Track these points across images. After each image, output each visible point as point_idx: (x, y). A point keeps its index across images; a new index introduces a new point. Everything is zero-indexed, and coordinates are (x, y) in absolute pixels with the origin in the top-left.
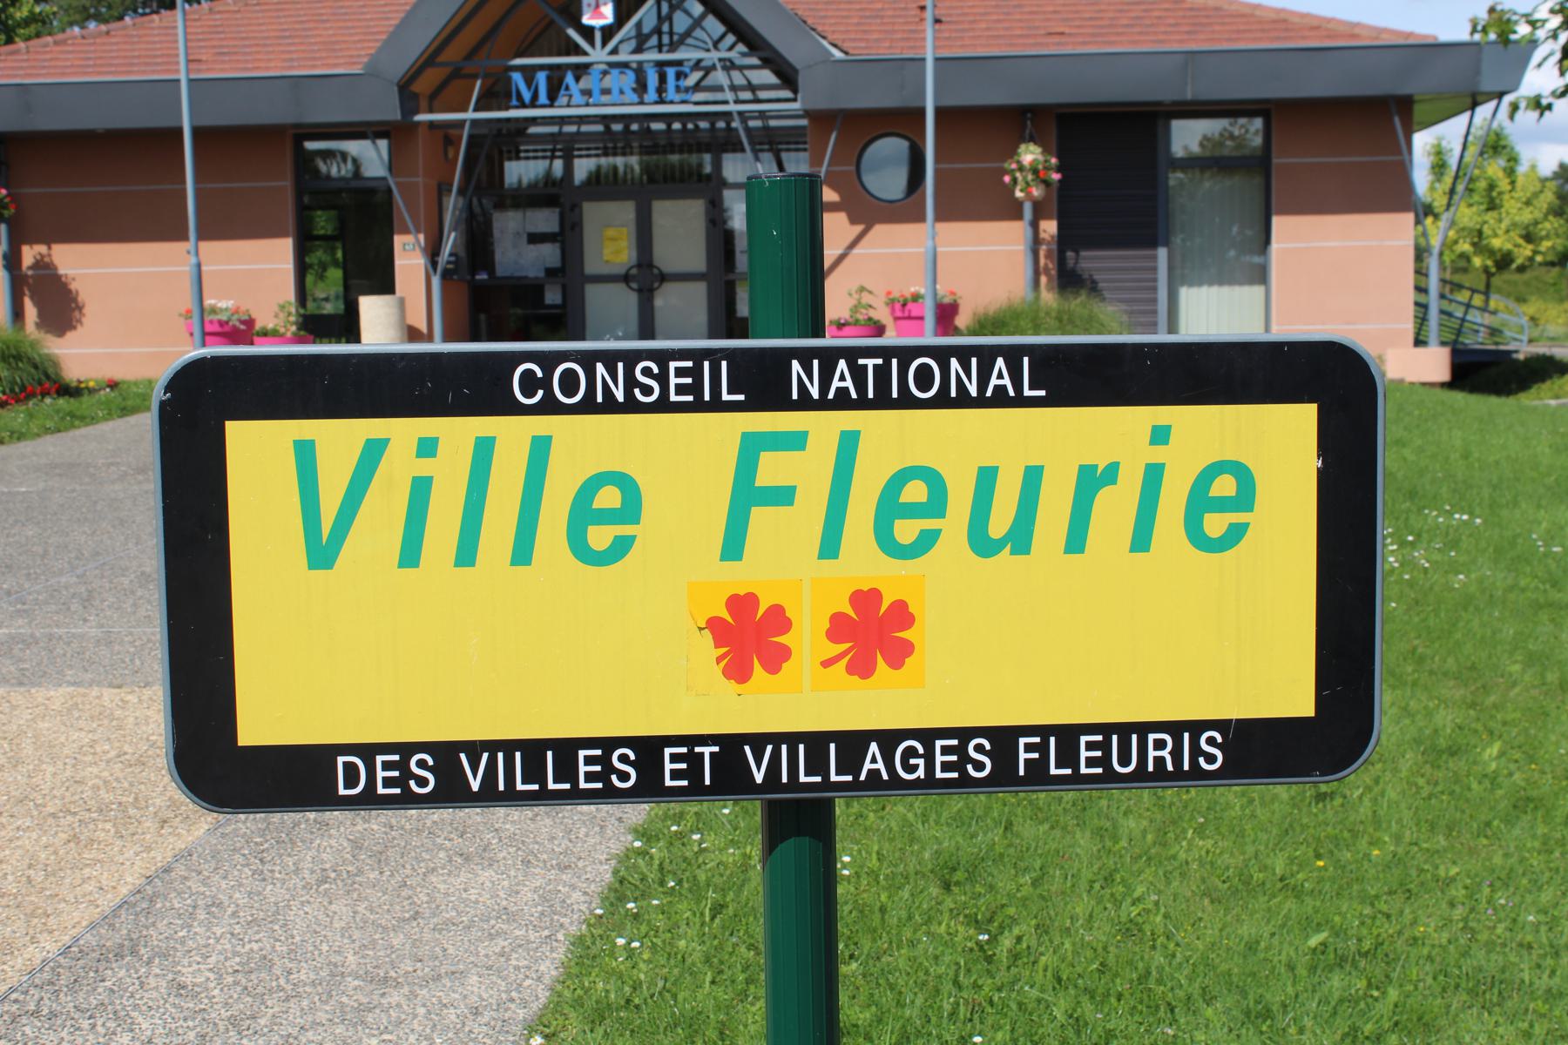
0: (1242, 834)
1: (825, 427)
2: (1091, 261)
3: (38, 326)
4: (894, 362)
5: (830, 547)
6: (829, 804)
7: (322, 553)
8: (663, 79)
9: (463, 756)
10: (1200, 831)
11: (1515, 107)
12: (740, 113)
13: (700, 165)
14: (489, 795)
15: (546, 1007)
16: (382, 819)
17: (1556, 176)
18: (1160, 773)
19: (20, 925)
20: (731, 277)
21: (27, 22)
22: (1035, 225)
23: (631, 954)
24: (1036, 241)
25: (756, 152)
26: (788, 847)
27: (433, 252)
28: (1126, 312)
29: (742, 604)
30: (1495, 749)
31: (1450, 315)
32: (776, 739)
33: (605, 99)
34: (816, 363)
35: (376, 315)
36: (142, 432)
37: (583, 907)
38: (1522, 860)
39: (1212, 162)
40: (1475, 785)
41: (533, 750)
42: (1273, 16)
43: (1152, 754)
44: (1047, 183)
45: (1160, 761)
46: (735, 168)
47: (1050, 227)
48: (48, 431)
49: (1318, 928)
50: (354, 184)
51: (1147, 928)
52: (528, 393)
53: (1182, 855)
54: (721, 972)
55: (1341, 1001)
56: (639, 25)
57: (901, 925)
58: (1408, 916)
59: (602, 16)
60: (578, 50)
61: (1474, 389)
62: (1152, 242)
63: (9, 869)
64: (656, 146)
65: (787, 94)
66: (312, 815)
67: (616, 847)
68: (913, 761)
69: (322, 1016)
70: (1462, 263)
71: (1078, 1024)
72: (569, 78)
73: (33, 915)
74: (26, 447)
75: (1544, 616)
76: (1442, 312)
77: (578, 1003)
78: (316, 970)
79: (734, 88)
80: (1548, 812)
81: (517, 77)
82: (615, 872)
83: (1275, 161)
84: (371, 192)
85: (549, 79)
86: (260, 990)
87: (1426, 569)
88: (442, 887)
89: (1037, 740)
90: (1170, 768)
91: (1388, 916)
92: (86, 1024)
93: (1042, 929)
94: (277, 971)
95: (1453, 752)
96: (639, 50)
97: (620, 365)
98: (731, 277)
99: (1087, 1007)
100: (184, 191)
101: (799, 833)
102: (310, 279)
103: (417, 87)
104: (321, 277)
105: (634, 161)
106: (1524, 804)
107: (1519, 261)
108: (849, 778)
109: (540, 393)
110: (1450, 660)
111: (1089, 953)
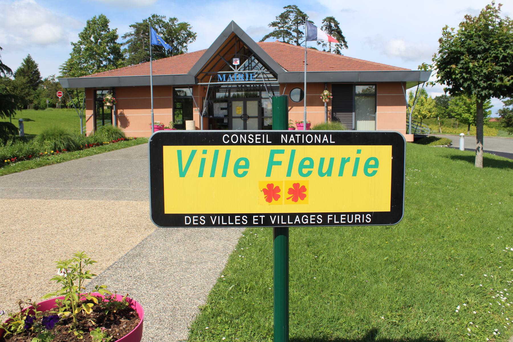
0: (370, 236)
1: (288, 149)
2: (339, 115)
3: (120, 126)
4: (303, 135)
5: (289, 174)
6: (288, 228)
7: (182, 174)
8: (249, 76)
9: (211, 217)
10: (362, 235)
11: (427, 84)
12: (265, 83)
13: (257, 94)
14: (216, 225)
15: (224, 269)
16: (190, 229)
17: (435, 99)
18: (358, 223)
19: (117, 249)
20: (263, 117)
21: (120, 65)
22: (327, 107)
23: (242, 259)
24: (327, 110)
25: (269, 91)
26: (279, 237)
27: (201, 112)
28: (346, 126)
29: (270, 186)
30: (423, 219)
31: (413, 127)
32: (277, 214)
33: (237, 80)
34: (286, 135)
35: (188, 123)
36: (146, 148)
37: (232, 249)
38: (429, 242)
39: (364, 95)
40: (419, 226)
41: (226, 216)
42: (377, 64)
43: (356, 219)
44: (329, 99)
45: (358, 220)
46: (264, 94)
47: (330, 108)
48: (122, 148)
49: (386, 256)
50: (185, 97)
51: (350, 255)
52: (226, 141)
53: (358, 240)
54: (261, 263)
55: (391, 271)
56: (245, 65)
57: (299, 254)
58: (405, 254)
59: (237, 63)
60: (232, 70)
61: (418, 143)
62: (351, 111)
63: (114, 238)
64: (248, 90)
65: (275, 79)
66: (176, 228)
67: (239, 236)
68: (305, 220)
69: (178, 270)
70: (416, 117)
71: (336, 275)
72: (230, 76)
73: (119, 247)
74: (118, 151)
75: (433, 191)
76: (412, 127)
77: (231, 269)
78: (177, 260)
79: (264, 78)
80: (434, 232)
81: (219, 75)
82: (239, 242)
83: (377, 95)
84: (188, 99)
85: (226, 76)
86: (165, 264)
87: (409, 181)
88: (203, 244)
89: (332, 215)
90: (360, 222)
91: (401, 253)
92: (130, 270)
93: (328, 255)
94: (169, 260)
95: (414, 219)
96: (244, 70)
97: (245, 135)
98: (263, 117)
99: (338, 272)
100: (151, 99)
101: (281, 234)
102: (175, 117)
103: (198, 77)
104: (178, 116)
105: (243, 93)
106: (429, 230)
107: (428, 117)
108: (292, 223)
109: (229, 141)
110: (414, 200)
111: (338, 260)
